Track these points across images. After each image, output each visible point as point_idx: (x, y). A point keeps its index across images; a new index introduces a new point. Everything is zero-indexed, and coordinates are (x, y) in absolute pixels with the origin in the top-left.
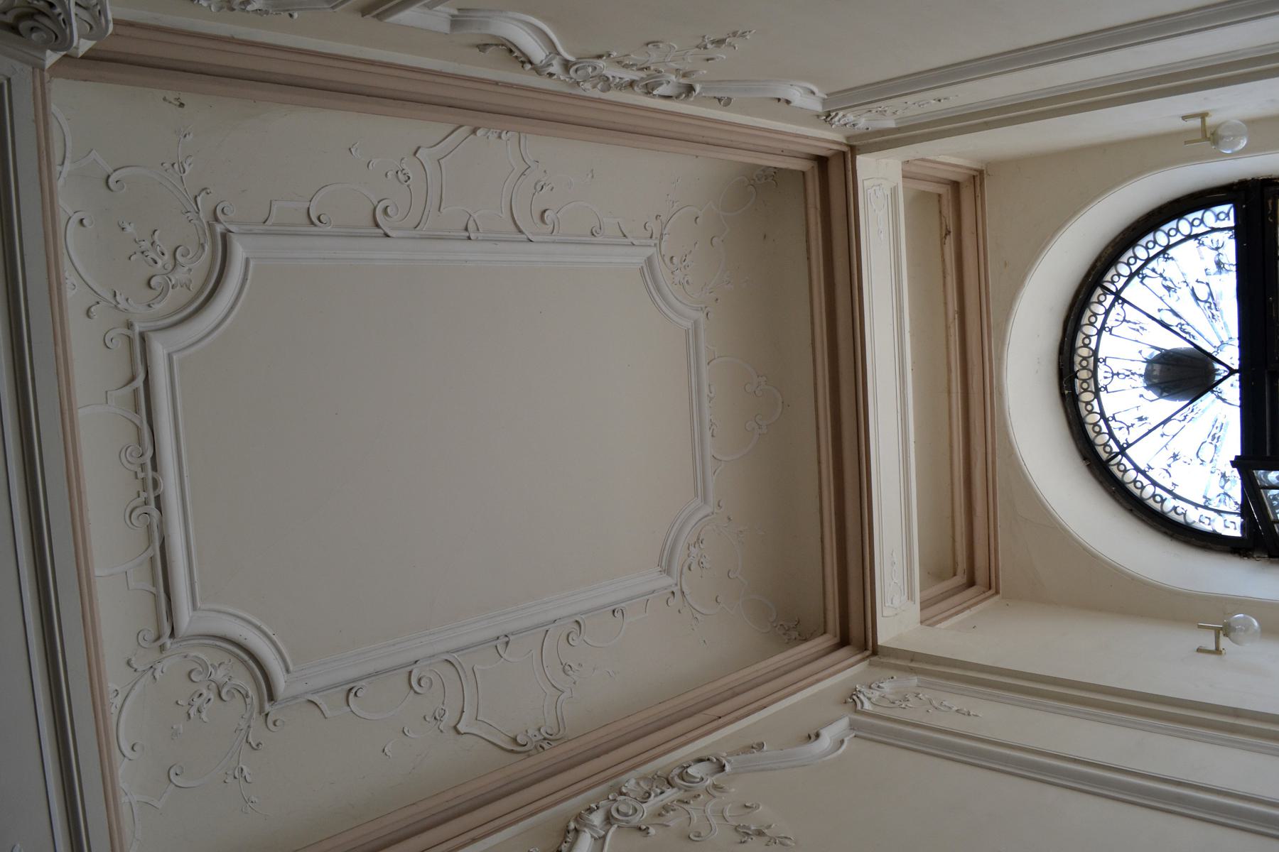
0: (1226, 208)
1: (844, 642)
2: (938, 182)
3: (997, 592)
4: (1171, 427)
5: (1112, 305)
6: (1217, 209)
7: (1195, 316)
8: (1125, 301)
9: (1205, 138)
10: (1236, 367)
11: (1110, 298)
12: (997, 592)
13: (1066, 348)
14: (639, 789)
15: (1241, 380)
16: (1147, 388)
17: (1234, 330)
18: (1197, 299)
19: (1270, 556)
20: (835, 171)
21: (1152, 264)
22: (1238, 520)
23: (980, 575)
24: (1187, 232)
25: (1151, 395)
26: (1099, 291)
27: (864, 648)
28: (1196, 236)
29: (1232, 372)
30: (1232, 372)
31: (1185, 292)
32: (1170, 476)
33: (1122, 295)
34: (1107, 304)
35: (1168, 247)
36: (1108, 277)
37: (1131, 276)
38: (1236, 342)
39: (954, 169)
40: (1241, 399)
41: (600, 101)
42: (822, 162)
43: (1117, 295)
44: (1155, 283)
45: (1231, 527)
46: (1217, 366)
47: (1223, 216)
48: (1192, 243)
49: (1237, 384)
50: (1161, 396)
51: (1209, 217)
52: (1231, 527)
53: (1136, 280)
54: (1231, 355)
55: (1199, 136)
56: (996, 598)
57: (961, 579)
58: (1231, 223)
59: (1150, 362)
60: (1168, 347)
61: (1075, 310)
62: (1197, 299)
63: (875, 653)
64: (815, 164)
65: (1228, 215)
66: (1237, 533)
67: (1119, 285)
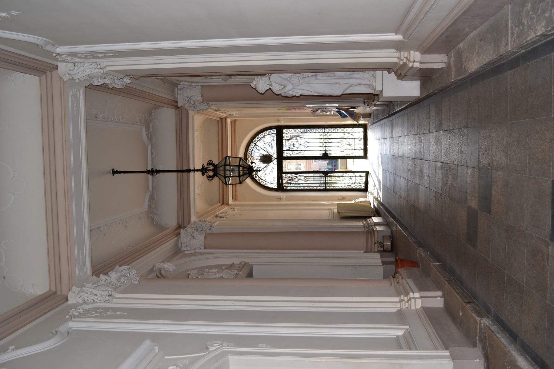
0: (275, 130)
1: (223, 204)
2: (174, 106)
3: (237, 200)
4: (265, 169)
5: (254, 146)
6: (273, 130)
7: (269, 149)
8: (257, 145)
9: (277, 121)
10: (276, 158)
11: (254, 145)
12: (237, 200)
13: (246, 153)
14: (117, 275)
15: (277, 160)
16: (261, 162)
17: (276, 152)
18: (269, 145)
19: (282, 191)
20: (224, 120)
21: (262, 139)
22: (276, 185)
23: (225, 201)
24: (268, 133)
25: (261, 163)
26: (252, 143)
27: (227, 204)
28: (269, 134)
29: (275, 159)
30: (275, 159)
31: (267, 144)
32: (353, 135)
33: (256, 144)
34: (253, 146)
35: (265, 136)
36: (254, 141)
37: (258, 141)
38: (276, 154)
39: (170, 100)
40: (277, 163)
41: (214, 113)
42: (221, 119)
43: (255, 144)
44: (262, 142)
45: (275, 186)
46: (273, 158)
47: (274, 131)
48: (269, 136)
49: (276, 161)
50: (263, 163)
51: (272, 131)
52: (275, 186)
53: (259, 141)
54: (275, 156)
55: (276, 120)
56: (237, 201)
57: (220, 204)
58: (275, 133)
59: (261, 157)
60: (265, 154)
61: (247, 147)
62: (269, 145)
63: (228, 205)
64: (221, 119)
65: (275, 131)
66: (276, 188)
67: (256, 142)
